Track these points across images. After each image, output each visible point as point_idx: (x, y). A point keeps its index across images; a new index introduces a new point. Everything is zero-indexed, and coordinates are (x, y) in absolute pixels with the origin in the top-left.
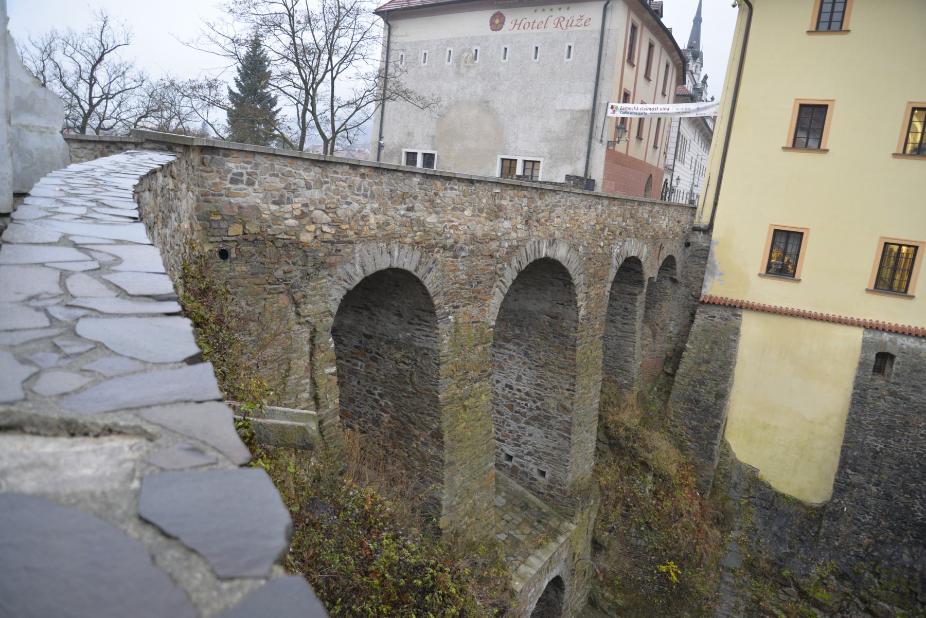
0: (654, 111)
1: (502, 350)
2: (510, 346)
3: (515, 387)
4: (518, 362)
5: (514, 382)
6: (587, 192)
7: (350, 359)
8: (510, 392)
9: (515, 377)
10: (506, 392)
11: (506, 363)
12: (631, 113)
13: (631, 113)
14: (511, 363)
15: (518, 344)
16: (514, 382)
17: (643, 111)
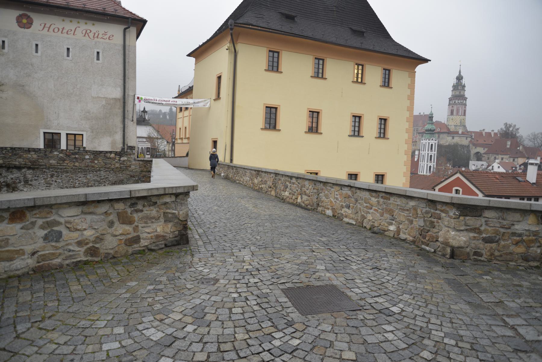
0: (168, 103)
17: (161, 102)
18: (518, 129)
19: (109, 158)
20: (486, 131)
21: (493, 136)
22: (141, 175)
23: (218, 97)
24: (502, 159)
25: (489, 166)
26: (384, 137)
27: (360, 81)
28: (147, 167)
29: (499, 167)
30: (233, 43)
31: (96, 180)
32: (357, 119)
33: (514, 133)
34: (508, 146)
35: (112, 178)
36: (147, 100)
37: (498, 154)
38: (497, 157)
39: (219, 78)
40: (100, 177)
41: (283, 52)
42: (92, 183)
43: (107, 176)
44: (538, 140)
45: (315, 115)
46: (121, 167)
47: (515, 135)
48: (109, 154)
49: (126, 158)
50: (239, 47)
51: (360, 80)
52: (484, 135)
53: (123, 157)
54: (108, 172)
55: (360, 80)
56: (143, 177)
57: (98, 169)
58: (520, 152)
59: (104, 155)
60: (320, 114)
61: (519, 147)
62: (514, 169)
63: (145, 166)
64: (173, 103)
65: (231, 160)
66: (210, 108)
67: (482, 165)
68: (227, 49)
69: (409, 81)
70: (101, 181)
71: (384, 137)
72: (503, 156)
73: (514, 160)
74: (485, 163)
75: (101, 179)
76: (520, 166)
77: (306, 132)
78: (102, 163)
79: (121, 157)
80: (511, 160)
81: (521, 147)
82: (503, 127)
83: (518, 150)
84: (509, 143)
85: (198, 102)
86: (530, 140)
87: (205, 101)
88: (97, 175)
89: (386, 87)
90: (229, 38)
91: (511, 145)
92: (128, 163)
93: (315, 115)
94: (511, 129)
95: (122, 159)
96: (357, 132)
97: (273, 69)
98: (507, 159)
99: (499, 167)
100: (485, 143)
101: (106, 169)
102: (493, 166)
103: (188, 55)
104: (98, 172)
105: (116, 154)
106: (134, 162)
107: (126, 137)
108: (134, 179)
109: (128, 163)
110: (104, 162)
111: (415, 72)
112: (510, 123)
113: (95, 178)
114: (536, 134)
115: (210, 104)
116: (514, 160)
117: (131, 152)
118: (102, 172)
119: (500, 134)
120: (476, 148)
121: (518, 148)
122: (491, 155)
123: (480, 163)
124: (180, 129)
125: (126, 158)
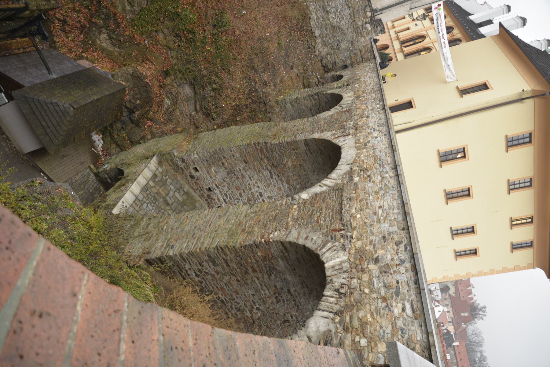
0: (442, 38)
1: (279, 182)
2: (286, 185)
3: (263, 197)
4: (280, 194)
5: (266, 196)
6: (379, 66)
7: (263, 285)
8: (258, 196)
9: (269, 195)
10: (256, 194)
11: (273, 187)
12: (437, 22)
13: (437, 22)
14: (276, 189)
15: (291, 190)
16: (266, 196)
17: (440, 31)
18: (482, 319)
19: (365, 11)
20: (473, 290)
21: (469, 296)
22: (356, 52)
23: (464, 92)
24: (448, 312)
25: (438, 301)
26: (457, 256)
27: (514, 223)
28: (367, 53)
29: (440, 311)
30: (535, 96)
31: (338, 8)
32: (472, 230)
33: (477, 316)
34: (462, 314)
35: (344, 23)
36: (439, 15)
37: (452, 306)
38: (449, 307)
39: (484, 87)
40: (342, 11)
41: (533, 147)
42: (333, 4)
43: (345, 17)
44: (476, 338)
45: (467, 193)
46: (358, 27)
47: (476, 318)
48: (369, 10)
49: (369, 29)
50: (530, 103)
51: (514, 223)
52: (468, 289)
53: (371, 25)
54: (349, 17)
55: (514, 223)
56: (355, 54)
57: (350, 5)
58: (460, 326)
59: (367, 5)
60: (468, 198)
61: (465, 324)
62: (442, 325)
63: (366, 51)
64: (443, 44)
65: (397, 132)
66: (446, 82)
67: (438, 296)
68: (523, 90)
69: (525, 265)
70: (338, 13)
71: (457, 256)
72: (451, 312)
73: (450, 322)
74: (440, 298)
75: (340, 12)
76: (446, 329)
77: (445, 190)
78: (358, 6)
79: (369, 23)
80: (450, 320)
81: (465, 326)
82: (481, 305)
83: (461, 324)
84: (466, 314)
85: (450, 69)
86: (474, 330)
87: (454, 75)
88: (343, 7)
89: (512, 247)
90: (538, 88)
91: (464, 316)
92: (365, 34)
93: (467, 193)
94: (481, 313)
95: (368, 25)
96: (456, 233)
97: (509, 142)
98: (449, 316)
99: (440, 311)
100: (460, 291)
101: (352, 14)
102: (439, 306)
103: (500, 23)
104: (346, 7)
105: (371, 17)
106: (368, 38)
107: (390, 9)
108: (350, 46)
109: (365, 34)
110: (359, 7)
111: (534, 268)
112: (487, 311)
113: (339, 6)
114: (481, 335)
115: (451, 82)
116: (450, 322)
117: (378, 32)
118: (347, 11)
119: (473, 303)
120: (453, 285)
121: (463, 324)
122: (450, 300)
123: (439, 292)
124: (408, 29)
125: (369, 29)
